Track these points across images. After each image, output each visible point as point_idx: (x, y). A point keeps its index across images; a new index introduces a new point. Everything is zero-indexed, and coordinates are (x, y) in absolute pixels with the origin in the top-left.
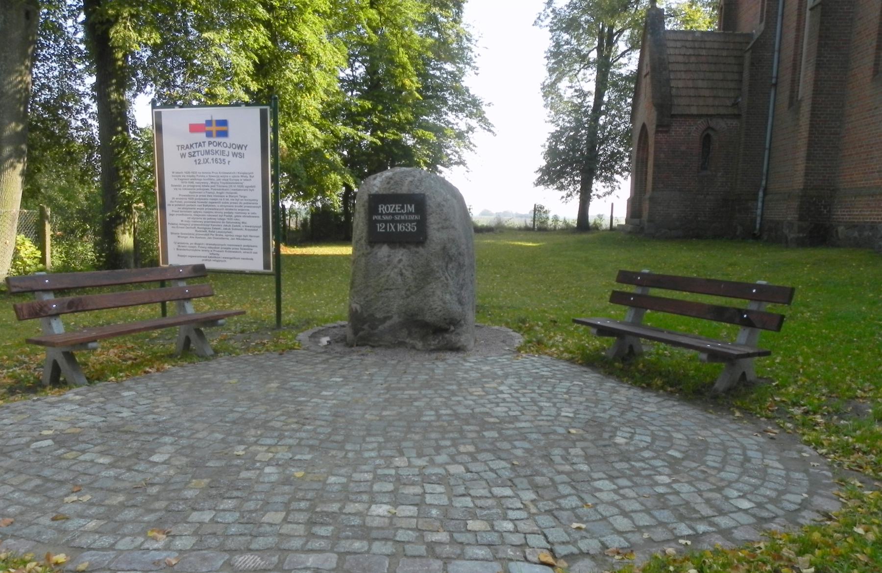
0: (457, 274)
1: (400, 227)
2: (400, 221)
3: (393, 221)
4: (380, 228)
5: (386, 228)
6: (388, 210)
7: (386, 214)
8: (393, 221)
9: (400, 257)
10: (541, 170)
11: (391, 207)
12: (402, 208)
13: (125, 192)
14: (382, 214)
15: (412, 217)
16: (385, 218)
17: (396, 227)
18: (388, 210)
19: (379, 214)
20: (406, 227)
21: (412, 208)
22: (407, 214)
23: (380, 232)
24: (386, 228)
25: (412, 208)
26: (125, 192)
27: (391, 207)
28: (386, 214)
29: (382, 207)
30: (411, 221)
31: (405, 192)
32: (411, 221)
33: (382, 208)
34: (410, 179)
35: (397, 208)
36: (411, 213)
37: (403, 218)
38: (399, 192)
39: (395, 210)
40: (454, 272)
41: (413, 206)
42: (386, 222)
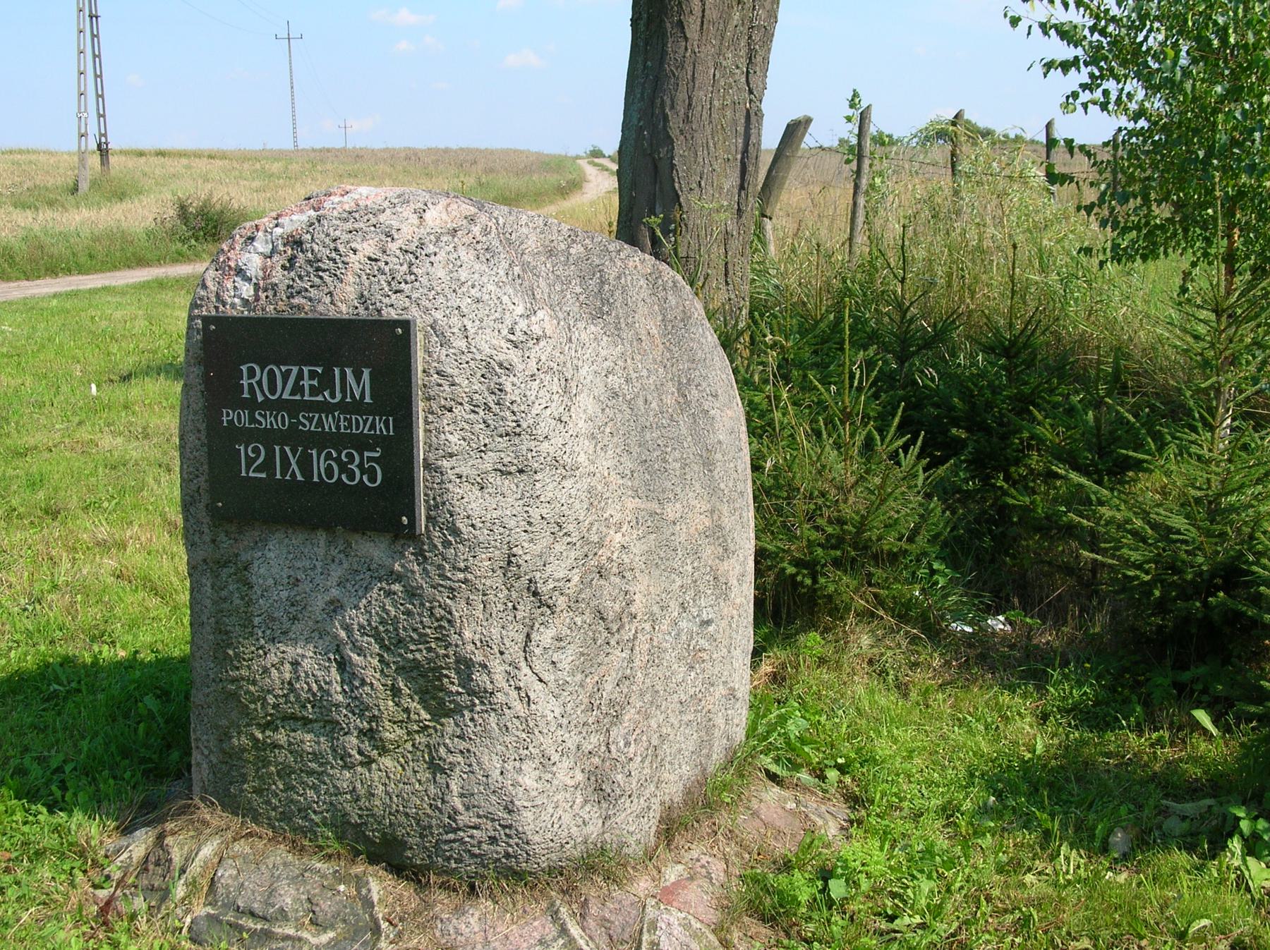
0: (586, 664)
1: (320, 465)
2: (323, 440)
3: (292, 436)
4: (250, 462)
5: (268, 465)
6: (273, 389)
7: (268, 405)
8: (292, 436)
9: (335, 592)
10: (1068, 45)
11: (365, 422)
12: (326, 382)
13: (1238, 819)
14: (252, 405)
15: (362, 426)
16: (267, 421)
17: (305, 464)
18: (273, 389)
19: (243, 404)
20: (343, 468)
21: (360, 385)
22: (343, 407)
23: (248, 478)
24: (268, 465)
25: (360, 385)
26: (1238, 819)
27: (365, 422)
28: (268, 405)
29: (252, 373)
30: (361, 443)
31: (344, 311)
32: (361, 443)
33: (253, 378)
34: (368, 248)
35: (306, 383)
36: (356, 407)
37: (329, 424)
38: (327, 310)
39: (297, 389)
40: (566, 659)
41: (366, 373)
42: (269, 437)
